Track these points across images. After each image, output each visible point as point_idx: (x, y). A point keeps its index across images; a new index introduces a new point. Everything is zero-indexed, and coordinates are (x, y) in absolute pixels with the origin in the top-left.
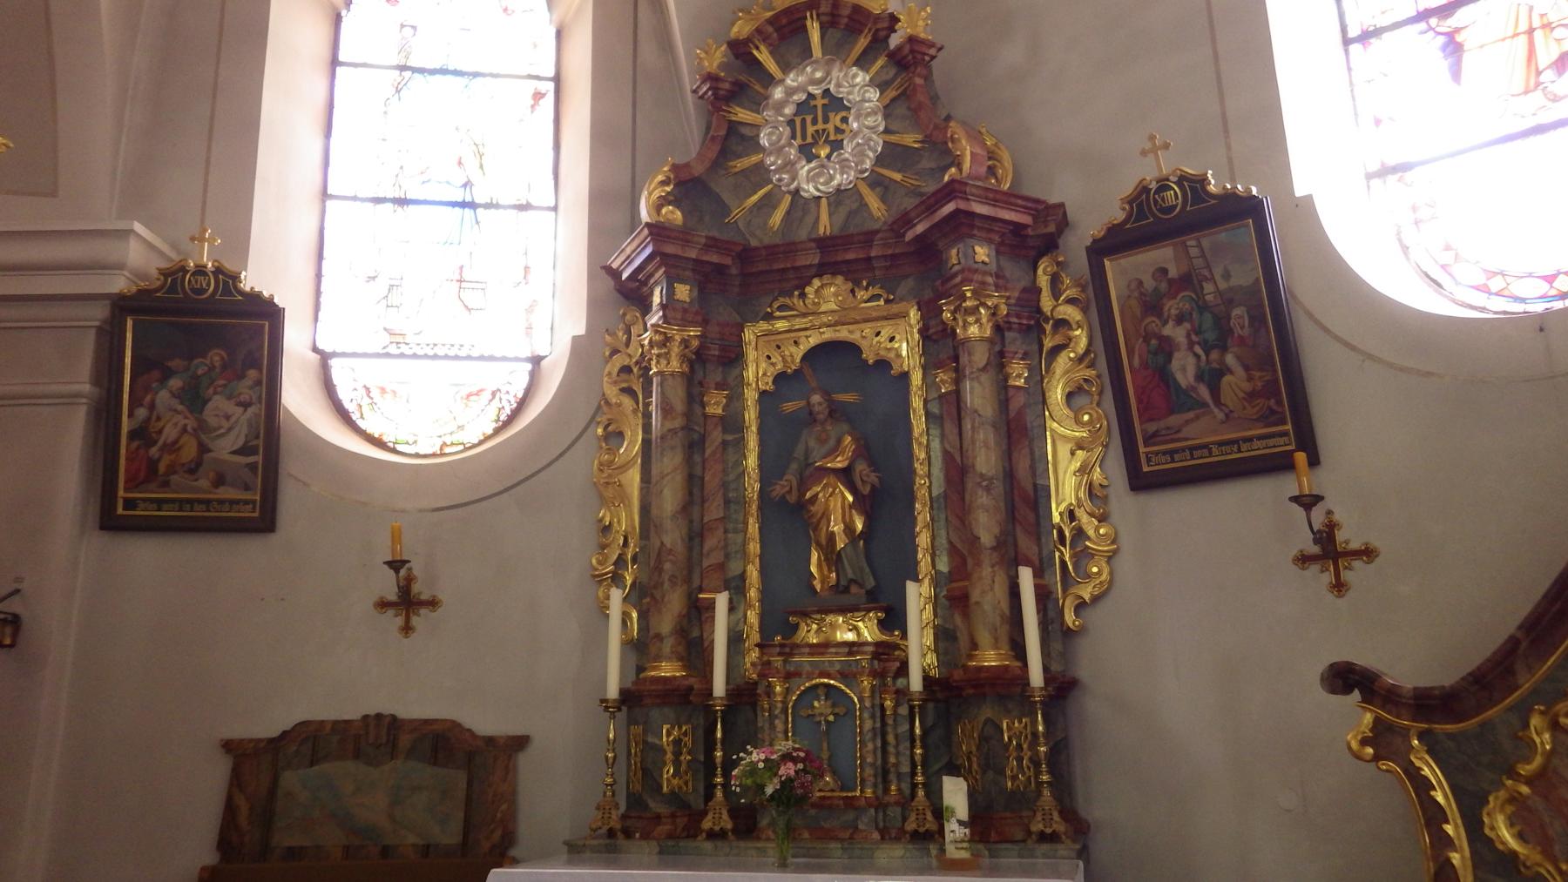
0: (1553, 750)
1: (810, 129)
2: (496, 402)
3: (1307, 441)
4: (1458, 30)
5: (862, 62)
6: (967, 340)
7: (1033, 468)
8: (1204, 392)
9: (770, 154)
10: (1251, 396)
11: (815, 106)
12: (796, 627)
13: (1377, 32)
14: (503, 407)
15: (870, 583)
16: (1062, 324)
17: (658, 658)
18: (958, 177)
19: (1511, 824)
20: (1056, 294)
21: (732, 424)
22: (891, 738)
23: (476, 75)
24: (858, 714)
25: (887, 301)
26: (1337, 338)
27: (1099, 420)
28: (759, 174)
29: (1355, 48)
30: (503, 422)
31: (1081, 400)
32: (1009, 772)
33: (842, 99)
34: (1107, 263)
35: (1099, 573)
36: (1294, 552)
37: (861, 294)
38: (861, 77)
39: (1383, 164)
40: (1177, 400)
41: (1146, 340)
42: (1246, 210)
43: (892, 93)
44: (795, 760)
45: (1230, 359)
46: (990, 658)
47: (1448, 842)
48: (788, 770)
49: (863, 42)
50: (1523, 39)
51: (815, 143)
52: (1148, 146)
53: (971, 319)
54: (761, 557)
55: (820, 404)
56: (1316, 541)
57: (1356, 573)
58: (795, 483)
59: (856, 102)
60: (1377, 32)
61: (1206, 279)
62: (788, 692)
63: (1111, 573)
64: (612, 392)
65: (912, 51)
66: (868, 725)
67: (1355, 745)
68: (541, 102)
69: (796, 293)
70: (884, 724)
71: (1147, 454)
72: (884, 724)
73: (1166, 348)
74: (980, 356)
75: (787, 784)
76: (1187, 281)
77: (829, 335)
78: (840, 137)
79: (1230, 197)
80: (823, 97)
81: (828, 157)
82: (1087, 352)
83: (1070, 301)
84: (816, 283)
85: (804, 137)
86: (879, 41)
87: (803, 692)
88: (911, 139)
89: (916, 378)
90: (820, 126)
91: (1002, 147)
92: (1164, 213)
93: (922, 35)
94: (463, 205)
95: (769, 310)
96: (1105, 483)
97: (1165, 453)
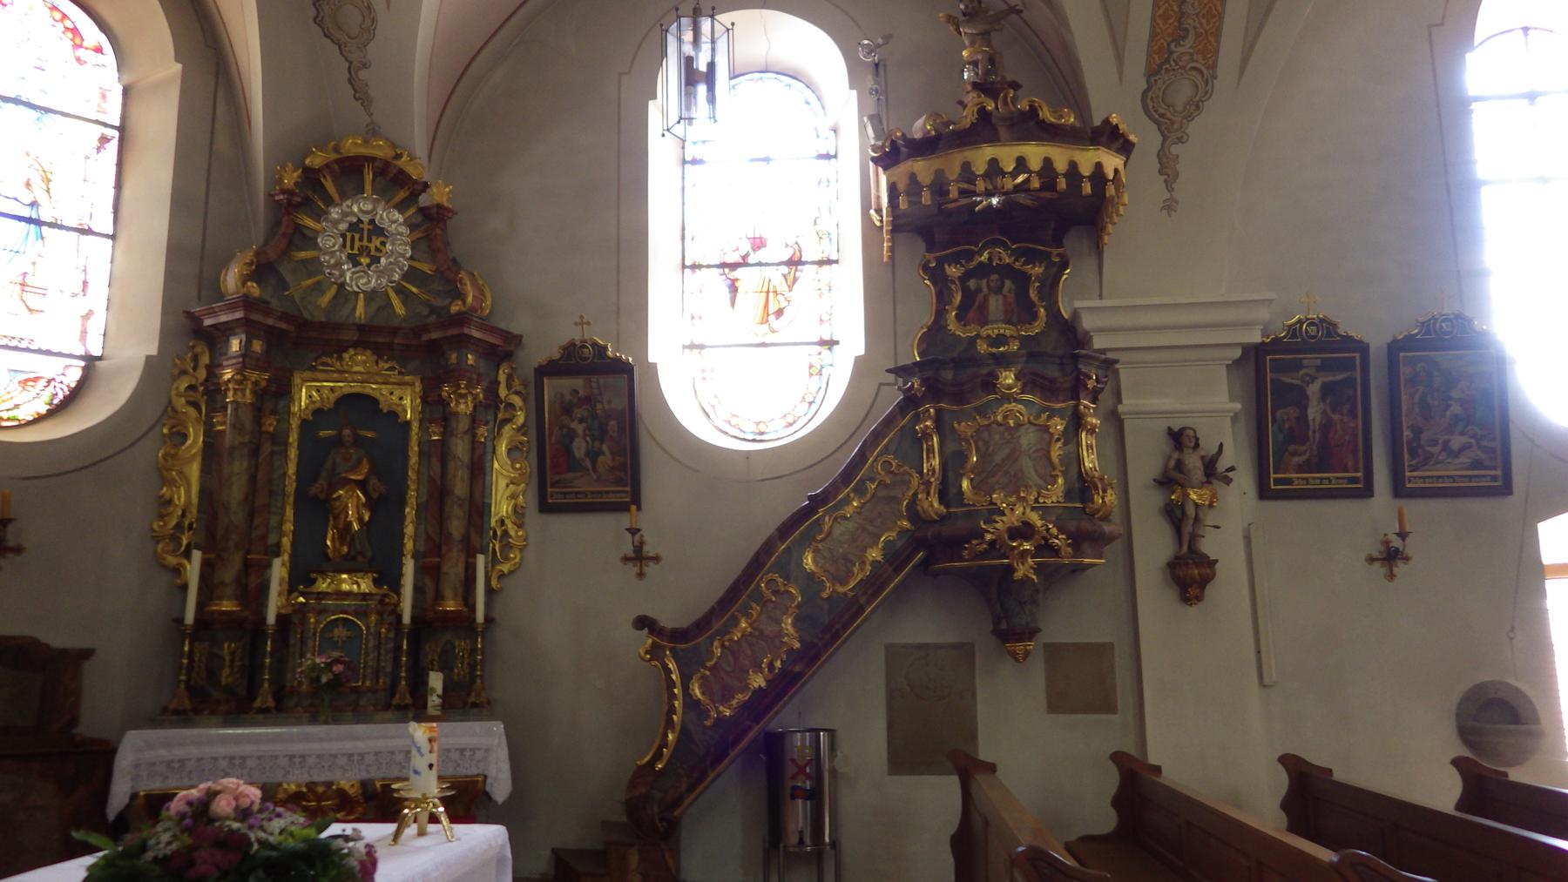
0: (720, 656)
1: (357, 244)
2: (50, 390)
3: (636, 499)
4: (737, 280)
5: (401, 207)
6: (456, 414)
7: (483, 492)
8: (588, 463)
9: (325, 254)
10: (613, 469)
11: (363, 229)
12: (314, 581)
13: (700, 267)
14: (56, 394)
15: (369, 554)
16: (510, 406)
17: (221, 598)
18: (463, 309)
19: (700, 687)
20: (509, 387)
21: (280, 440)
22: (382, 651)
23: (47, 110)
24: (364, 636)
25: (400, 373)
26: (658, 444)
27: (525, 469)
28: (312, 266)
29: (687, 271)
30: (56, 405)
31: (516, 454)
32: (456, 671)
33: (383, 228)
34: (545, 381)
35: (515, 558)
36: (622, 555)
37: (381, 364)
38: (397, 215)
39: (692, 342)
40: (572, 464)
41: (561, 428)
42: (625, 369)
43: (418, 234)
44: (341, 663)
45: (604, 447)
46: (450, 606)
47: (674, 696)
48: (338, 668)
49: (402, 194)
50: (764, 295)
51: (360, 254)
52: (579, 320)
53: (462, 401)
54: (294, 532)
55: (349, 436)
56: (634, 552)
57: (651, 569)
58: (325, 486)
59: (393, 234)
60: (700, 267)
61: (599, 401)
62: (317, 622)
63: (521, 559)
64: (180, 403)
65: (438, 213)
66: (371, 643)
67: (642, 654)
68: (106, 146)
69: (335, 356)
70: (380, 643)
71: (551, 492)
72: (380, 643)
73: (572, 435)
74: (464, 425)
75: (336, 677)
76: (588, 400)
77: (356, 388)
78: (378, 254)
79: (618, 360)
80: (369, 224)
81: (369, 266)
82: (524, 425)
83: (517, 393)
84: (352, 351)
85: (352, 248)
86: (413, 197)
87: (328, 623)
88: (426, 268)
89: (415, 426)
90: (365, 243)
91: (486, 286)
92: (581, 359)
93: (446, 204)
94: (29, 220)
95: (314, 364)
96: (524, 505)
97: (561, 493)
